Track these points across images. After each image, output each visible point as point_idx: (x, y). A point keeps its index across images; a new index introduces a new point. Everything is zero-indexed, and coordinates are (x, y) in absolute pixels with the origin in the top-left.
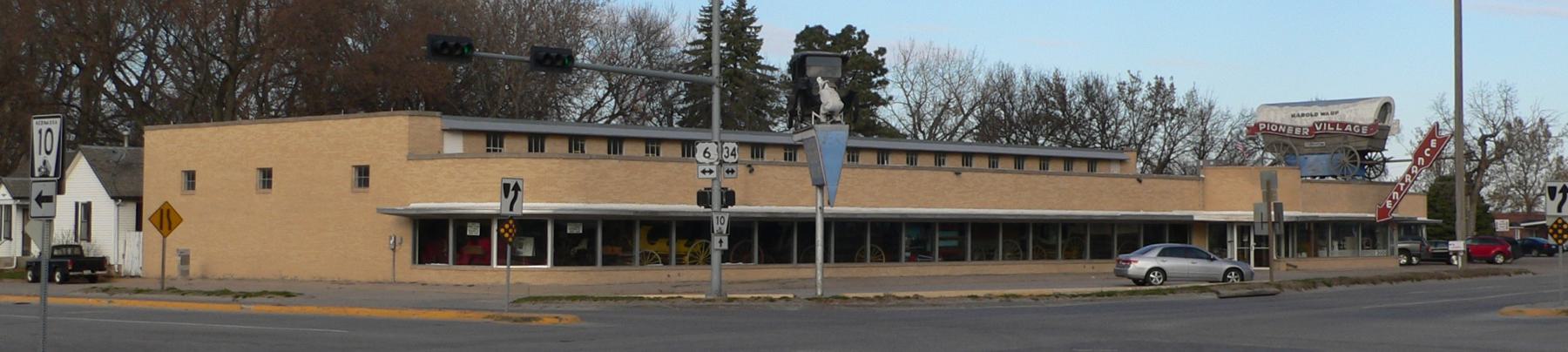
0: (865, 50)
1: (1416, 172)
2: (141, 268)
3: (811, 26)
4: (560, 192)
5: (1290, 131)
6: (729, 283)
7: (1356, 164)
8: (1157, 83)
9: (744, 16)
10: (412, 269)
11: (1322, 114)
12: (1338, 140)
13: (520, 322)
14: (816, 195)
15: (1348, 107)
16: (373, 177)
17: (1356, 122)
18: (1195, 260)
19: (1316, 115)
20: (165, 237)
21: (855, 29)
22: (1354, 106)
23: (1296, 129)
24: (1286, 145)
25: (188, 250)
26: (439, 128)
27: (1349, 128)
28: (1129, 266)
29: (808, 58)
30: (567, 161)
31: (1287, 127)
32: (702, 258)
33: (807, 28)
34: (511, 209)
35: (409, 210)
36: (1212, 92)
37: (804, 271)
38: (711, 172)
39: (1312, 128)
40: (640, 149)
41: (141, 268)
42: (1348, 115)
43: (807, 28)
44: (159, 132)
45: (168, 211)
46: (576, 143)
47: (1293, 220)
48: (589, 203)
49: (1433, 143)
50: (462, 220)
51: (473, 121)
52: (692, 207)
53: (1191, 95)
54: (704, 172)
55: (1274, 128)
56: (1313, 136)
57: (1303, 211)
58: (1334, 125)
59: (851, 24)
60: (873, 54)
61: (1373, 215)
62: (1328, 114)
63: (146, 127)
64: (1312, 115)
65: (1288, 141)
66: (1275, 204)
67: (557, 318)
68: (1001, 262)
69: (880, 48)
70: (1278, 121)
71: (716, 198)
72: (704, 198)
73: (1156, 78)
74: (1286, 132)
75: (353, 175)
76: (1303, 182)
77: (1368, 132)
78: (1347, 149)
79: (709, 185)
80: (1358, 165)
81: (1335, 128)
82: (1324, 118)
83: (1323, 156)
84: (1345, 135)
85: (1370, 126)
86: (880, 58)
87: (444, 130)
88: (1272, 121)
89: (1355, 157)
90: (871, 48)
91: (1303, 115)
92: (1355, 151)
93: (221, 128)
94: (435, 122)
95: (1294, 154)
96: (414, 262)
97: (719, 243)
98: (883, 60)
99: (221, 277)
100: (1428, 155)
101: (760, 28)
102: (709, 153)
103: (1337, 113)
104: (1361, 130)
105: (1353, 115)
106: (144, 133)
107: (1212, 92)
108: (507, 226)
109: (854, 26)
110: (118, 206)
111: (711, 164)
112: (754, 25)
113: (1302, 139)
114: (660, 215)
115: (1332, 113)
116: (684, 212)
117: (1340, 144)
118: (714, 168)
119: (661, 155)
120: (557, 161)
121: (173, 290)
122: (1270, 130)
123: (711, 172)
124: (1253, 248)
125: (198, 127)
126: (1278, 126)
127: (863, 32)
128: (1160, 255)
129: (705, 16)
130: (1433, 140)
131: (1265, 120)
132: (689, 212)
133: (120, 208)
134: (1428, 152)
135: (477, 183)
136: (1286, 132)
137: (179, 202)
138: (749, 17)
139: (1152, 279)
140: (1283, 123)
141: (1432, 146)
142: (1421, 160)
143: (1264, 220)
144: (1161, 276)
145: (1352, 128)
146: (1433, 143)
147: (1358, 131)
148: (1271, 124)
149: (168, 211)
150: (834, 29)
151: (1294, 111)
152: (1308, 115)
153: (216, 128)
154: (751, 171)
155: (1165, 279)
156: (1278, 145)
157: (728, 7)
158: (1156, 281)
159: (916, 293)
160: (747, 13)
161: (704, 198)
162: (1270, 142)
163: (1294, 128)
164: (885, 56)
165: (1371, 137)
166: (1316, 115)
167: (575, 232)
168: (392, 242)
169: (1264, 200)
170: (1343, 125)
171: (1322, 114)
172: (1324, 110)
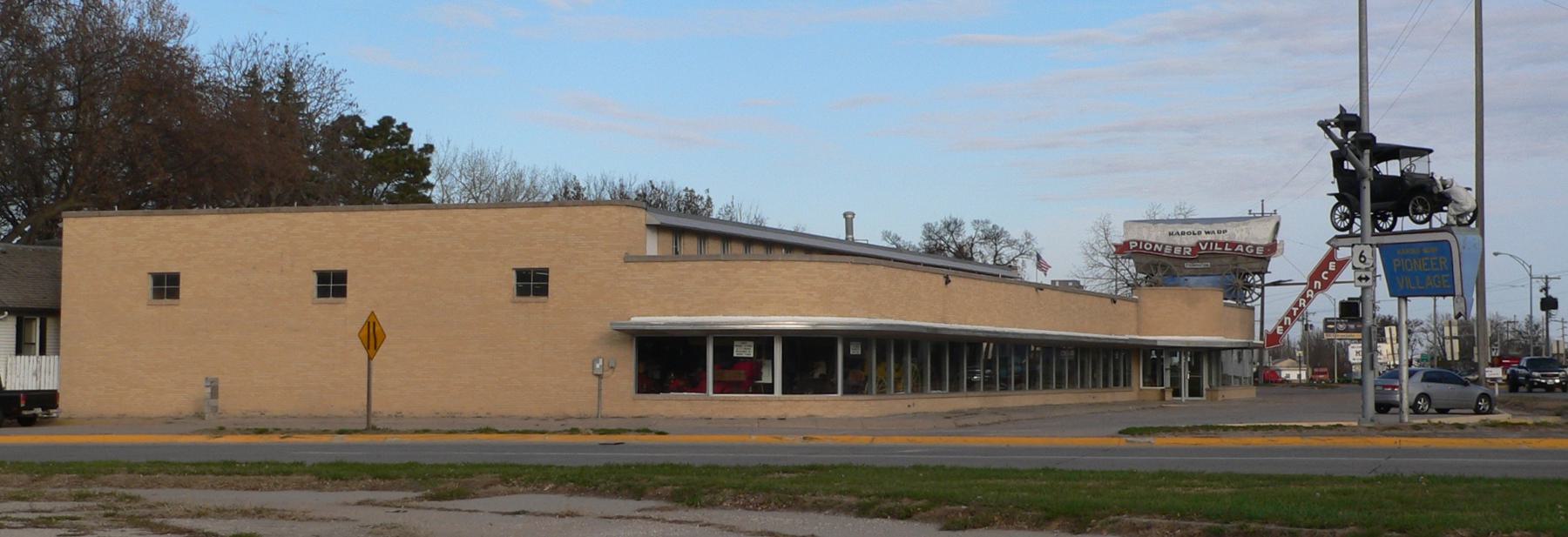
1: (1312, 296)
5: (1168, 250)
6: (526, 419)
8: (686, 195)
10: (634, 400)
11: (1207, 233)
12: (1226, 261)
15: (1239, 225)
17: (1247, 242)
19: (1199, 233)
20: (370, 359)
21: (394, 121)
22: (1243, 225)
23: (1258, 248)
24: (1164, 266)
26: (644, 222)
31: (1164, 246)
35: (631, 324)
36: (757, 207)
39: (1196, 248)
42: (1238, 234)
49: (1332, 266)
50: (725, 340)
55: (1148, 246)
56: (1197, 256)
58: (1222, 244)
62: (1213, 232)
64: (1194, 234)
69: (426, 145)
74: (1163, 251)
81: (1224, 248)
82: (1209, 238)
83: (1206, 277)
84: (1235, 256)
87: (649, 226)
88: (1145, 239)
90: (417, 141)
91: (1183, 233)
95: (1175, 276)
99: (582, 416)
100: (1326, 278)
102: (1364, 257)
103: (1225, 231)
104: (1255, 251)
105: (1245, 235)
107: (757, 207)
109: (394, 117)
111: (1367, 269)
113: (1183, 259)
115: (1219, 232)
122: (1143, 249)
126: (1154, 244)
127: (404, 125)
130: (1331, 263)
131: (1135, 237)
134: (1326, 275)
135: (755, 292)
136: (1163, 251)
139: (1420, 405)
141: (1330, 269)
142: (1317, 284)
145: (1244, 249)
146: (1332, 266)
147: (1252, 251)
148: (1144, 243)
149: (374, 324)
150: (371, 121)
151: (1171, 228)
152: (1189, 233)
153: (224, 217)
160: (296, 96)
163: (1173, 247)
166: (1199, 233)
168: (598, 366)
170: (1233, 245)
171: (1207, 233)
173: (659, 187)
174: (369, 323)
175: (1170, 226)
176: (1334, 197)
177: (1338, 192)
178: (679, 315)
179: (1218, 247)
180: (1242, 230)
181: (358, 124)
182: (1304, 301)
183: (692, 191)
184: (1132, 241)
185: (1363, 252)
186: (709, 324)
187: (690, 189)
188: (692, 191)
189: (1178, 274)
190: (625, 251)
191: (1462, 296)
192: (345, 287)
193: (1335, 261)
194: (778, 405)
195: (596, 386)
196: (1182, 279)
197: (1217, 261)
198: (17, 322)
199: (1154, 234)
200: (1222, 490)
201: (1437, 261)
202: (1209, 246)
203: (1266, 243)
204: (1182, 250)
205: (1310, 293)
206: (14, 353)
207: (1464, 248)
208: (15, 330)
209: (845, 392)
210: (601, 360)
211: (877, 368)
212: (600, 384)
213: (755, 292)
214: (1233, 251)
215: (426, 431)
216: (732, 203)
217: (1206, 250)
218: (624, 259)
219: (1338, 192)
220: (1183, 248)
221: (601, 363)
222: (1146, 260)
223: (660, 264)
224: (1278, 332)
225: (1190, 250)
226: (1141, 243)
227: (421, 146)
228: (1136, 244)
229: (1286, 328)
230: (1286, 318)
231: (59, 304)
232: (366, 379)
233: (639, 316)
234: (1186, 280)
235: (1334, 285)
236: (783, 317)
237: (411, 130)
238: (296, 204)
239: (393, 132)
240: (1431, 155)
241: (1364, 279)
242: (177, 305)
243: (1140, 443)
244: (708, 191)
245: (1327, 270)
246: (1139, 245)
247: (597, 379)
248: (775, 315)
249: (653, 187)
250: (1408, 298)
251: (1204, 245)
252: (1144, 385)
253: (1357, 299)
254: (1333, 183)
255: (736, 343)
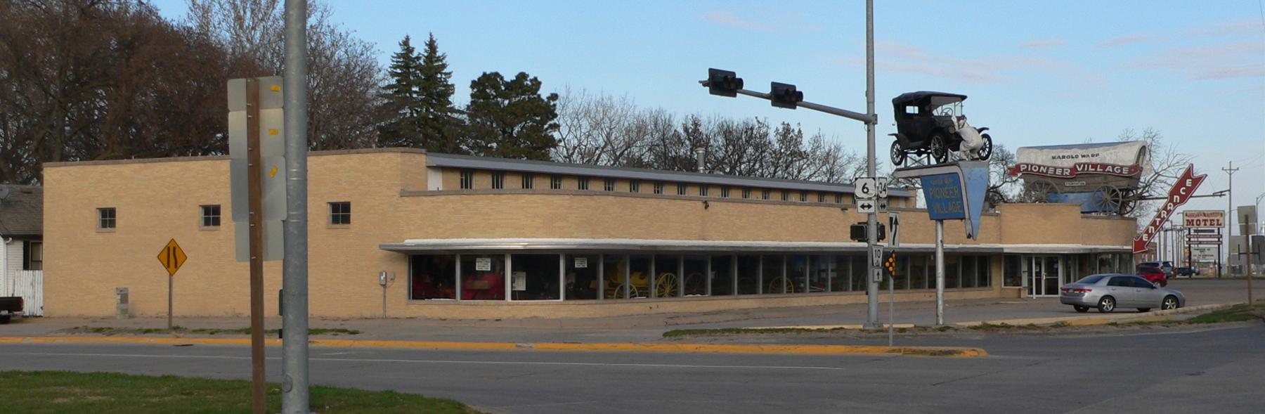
0: (539, 96)
1: (1172, 208)
2: (42, 308)
3: (488, 73)
4: (570, 227)
5: (1051, 171)
7: (1118, 202)
8: (784, 128)
9: (436, 61)
10: (407, 304)
11: (1083, 156)
12: (1098, 179)
13: (939, 355)
14: (936, 230)
15: (1108, 150)
16: (120, 220)
17: (1116, 163)
18: (1139, 289)
19: (1077, 157)
20: (171, 275)
21: (528, 76)
23: (1057, 170)
24: (1047, 184)
25: (127, 289)
26: (424, 164)
27: (1109, 169)
28: (1083, 295)
29: (932, 98)
30: (577, 197)
31: (1048, 168)
32: (668, 289)
33: (485, 74)
34: (894, 244)
37: (860, 297)
38: (869, 206)
39: (1074, 169)
40: (546, 183)
41: (42, 308)
42: (1108, 157)
43: (485, 74)
44: (63, 168)
45: (174, 248)
46: (556, 179)
47: (1087, 252)
48: (594, 238)
50: (470, 257)
51: (96, 164)
52: (848, 244)
53: (817, 141)
54: (863, 207)
55: (1035, 168)
56: (1074, 176)
57: (1082, 244)
58: (1095, 166)
59: (524, 71)
60: (546, 100)
61: (1130, 247)
63: (44, 164)
64: (1073, 157)
65: (1049, 181)
66: (1253, 237)
67: (974, 350)
68: (785, 294)
69: (552, 94)
70: (1039, 163)
71: (873, 232)
72: (858, 232)
73: (783, 124)
75: (97, 217)
76: (1082, 218)
77: (1130, 172)
78: (1108, 188)
79: (864, 220)
80: (1120, 202)
81: (1096, 168)
82: (1084, 160)
83: (1083, 194)
84: (1105, 175)
85: (1130, 168)
86: (552, 103)
87: (429, 167)
88: (1033, 162)
89: (1117, 195)
90: (544, 93)
91: (1063, 157)
92: (1117, 189)
93: (149, 164)
94: (420, 159)
95: (1056, 193)
96: (410, 298)
97: (875, 275)
98: (555, 105)
100: (1184, 193)
101: (450, 73)
102: (867, 189)
103: (1097, 155)
104: (1122, 171)
106: (42, 170)
108: (891, 260)
109: (527, 73)
110: (7, 244)
111: (870, 199)
112: (445, 71)
114: (825, 250)
115: (1093, 156)
116: (675, 246)
117: (1100, 183)
118: (872, 203)
119: (589, 189)
120: (567, 197)
121: (177, 328)
122: (1031, 171)
123: (869, 206)
124: (1044, 278)
125: (119, 163)
126: (1040, 167)
127: (536, 79)
128: (1110, 284)
129: (397, 62)
131: (1025, 161)
132: (678, 246)
133: (9, 246)
134: (1183, 191)
137: (193, 237)
138: (440, 63)
139: (1104, 305)
140: (1044, 164)
141: (1187, 185)
143: (1241, 252)
144: (1111, 303)
145: (1113, 170)
146: (1189, 183)
147: (1119, 171)
148: (1032, 166)
149: (174, 248)
150: (509, 76)
152: (1068, 157)
154: (707, 207)
155: (1114, 307)
156: (1040, 184)
157: (419, 54)
158: (1107, 308)
159: (1003, 321)
160: (439, 59)
161: (858, 232)
162: (1033, 181)
163: (1055, 169)
164: (557, 102)
165: (1131, 177)
166: (1077, 157)
167: (581, 266)
168: (382, 278)
169: (1241, 233)
170: (1104, 166)
171: (1083, 156)
172: (1084, 152)
173: (763, 122)
174: (169, 248)
175: (1054, 151)
176: (894, 137)
177: (897, 132)
178: (437, 238)
179: (1092, 168)
180: (1111, 154)
181: (498, 79)
182: (1166, 212)
183: (788, 125)
184: (1022, 164)
185: (866, 184)
186: (444, 245)
187: (786, 123)
188: (788, 125)
189: (1059, 192)
190: (400, 188)
191: (970, 219)
192: (219, 218)
193: (1191, 178)
194: (509, 310)
195: (382, 293)
196: (1063, 195)
197: (1091, 180)
198: (24, 245)
199: (1040, 159)
200: (82, 400)
201: (953, 190)
202: (1084, 167)
203: (1131, 164)
204: (1063, 171)
205: (1170, 206)
206: (22, 268)
207: (969, 179)
208: (22, 251)
209: (568, 297)
210: (384, 274)
211: (630, 277)
212: (385, 293)
213: (489, 219)
214: (1104, 171)
215: (148, 331)
216: (819, 133)
217: (1082, 171)
218: (400, 193)
219: (897, 132)
220: (1063, 169)
221: (384, 275)
222: (1033, 180)
223: (424, 198)
224: (1144, 239)
225: (1069, 171)
226: (1030, 166)
227: (548, 95)
228: (1026, 167)
229: (1150, 235)
230: (1150, 227)
231: (41, 230)
232: (168, 290)
233: (410, 239)
234: (1067, 196)
235: (1191, 199)
236: (511, 239)
237: (540, 83)
238: (200, 154)
239: (527, 84)
240: (964, 102)
241: (867, 206)
242: (114, 232)
243: (525, 347)
244: (799, 124)
245: (1185, 186)
246: (1028, 167)
247: (382, 288)
248: (505, 237)
249: (758, 122)
250: (944, 221)
251: (1080, 167)
252: (1005, 285)
253: (864, 223)
254: (893, 125)
255: (478, 259)
